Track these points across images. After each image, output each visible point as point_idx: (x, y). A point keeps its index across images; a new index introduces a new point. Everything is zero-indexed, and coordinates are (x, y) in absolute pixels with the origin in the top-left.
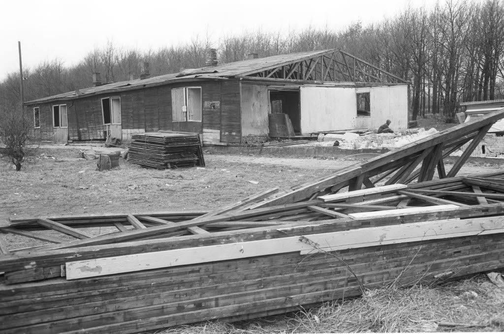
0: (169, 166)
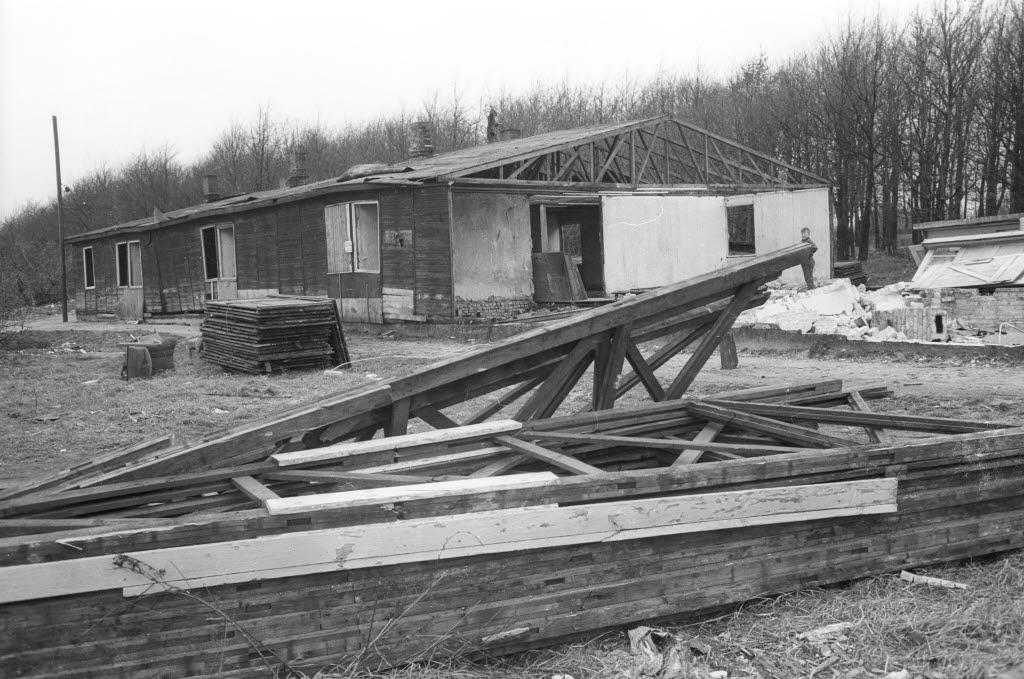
0: (269, 368)
